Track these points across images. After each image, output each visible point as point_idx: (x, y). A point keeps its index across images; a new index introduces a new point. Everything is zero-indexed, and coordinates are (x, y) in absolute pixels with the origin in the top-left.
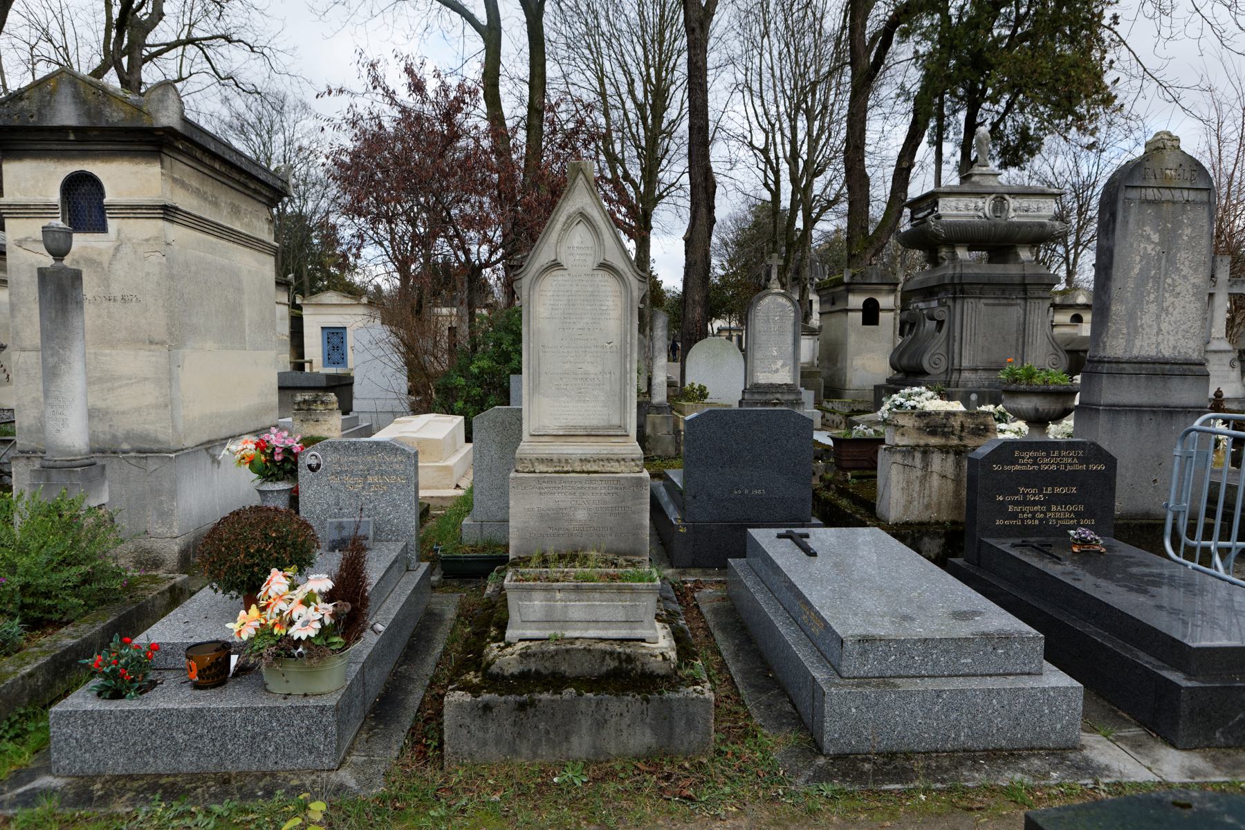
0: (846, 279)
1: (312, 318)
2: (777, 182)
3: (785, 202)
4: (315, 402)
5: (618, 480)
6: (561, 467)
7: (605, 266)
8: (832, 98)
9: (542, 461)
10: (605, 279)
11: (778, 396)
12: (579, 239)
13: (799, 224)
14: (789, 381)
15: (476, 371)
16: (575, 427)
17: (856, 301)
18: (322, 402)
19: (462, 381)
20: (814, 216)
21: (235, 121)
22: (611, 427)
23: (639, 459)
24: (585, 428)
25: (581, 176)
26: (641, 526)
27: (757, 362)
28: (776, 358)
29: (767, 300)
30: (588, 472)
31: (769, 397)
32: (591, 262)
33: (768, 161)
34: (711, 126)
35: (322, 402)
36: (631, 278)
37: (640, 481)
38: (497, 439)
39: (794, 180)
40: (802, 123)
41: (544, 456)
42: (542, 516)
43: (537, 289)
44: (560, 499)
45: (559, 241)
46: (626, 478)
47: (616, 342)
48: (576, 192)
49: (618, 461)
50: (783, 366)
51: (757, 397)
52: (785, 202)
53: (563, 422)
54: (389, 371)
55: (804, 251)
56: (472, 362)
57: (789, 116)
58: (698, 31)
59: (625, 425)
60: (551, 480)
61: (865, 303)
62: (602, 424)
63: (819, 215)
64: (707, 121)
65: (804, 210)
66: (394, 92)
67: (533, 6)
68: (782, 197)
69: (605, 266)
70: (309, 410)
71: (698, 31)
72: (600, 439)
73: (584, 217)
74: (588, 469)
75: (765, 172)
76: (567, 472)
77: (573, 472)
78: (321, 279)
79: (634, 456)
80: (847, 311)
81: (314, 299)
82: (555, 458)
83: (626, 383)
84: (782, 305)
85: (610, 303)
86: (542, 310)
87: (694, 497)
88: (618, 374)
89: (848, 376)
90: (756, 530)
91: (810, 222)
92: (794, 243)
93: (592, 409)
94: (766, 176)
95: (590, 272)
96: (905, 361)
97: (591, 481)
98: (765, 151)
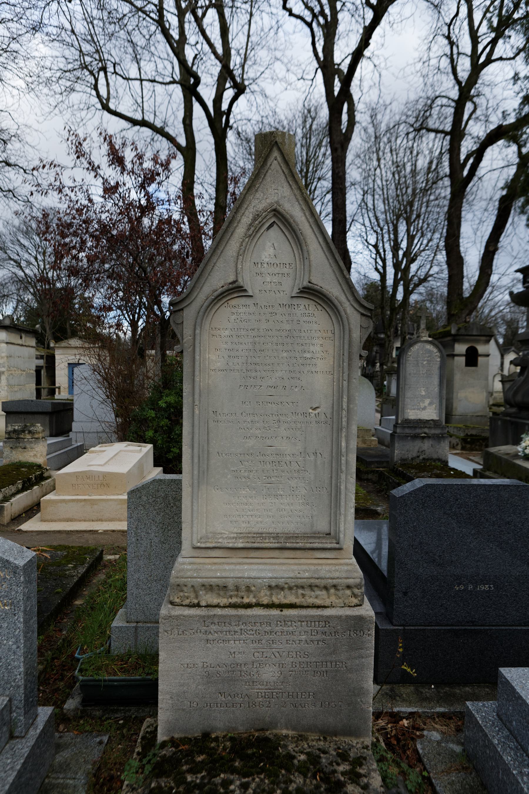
0: (453, 332)
1: (62, 356)
2: (384, 267)
3: (390, 281)
4: (23, 431)
5: (327, 620)
6: (239, 599)
7: (310, 292)
8: (423, 209)
9: (210, 588)
10: (307, 309)
11: (426, 430)
12: (271, 251)
13: (400, 296)
14: (435, 417)
15: (164, 405)
16: (260, 534)
17: (461, 348)
18: (30, 432)
19: (152, 414)
20: (410, 289)
21: (22, 226)
22: (315, 535)
23: (358, 586)
24: (276, 536)
25: (276, 154)
26: (360, 692)
27: (408, 401)
28: (424, 397)
29: (416, 347)
30: (281, 606)
31: (418, 431)
32: (289, 286)
33: (378, 252)
34: (349, 219)
35: (30, 432)
36: (350, 310)
37: (359, 622)
38: (158, 519)
39: (397, 266)
40: (402, 228)
41: (214, 581)
42: (209, 675)
43: (207, 326)
44: (234, 648)
45: (241, 253)
46: (339, 618)
47: (325, 407)
48: (268, 178)
49: (326, 588)
50: (430, 404)
51: (407, 431)
52: (390, 281)
53: (244, 528)
54: (95, 403)
55: (404, 313)
56: (161, 398)
57: (393, 223)
58: (339, 150)
59: (337, 532)
60: (224, 620)
61: (468, 350)
62: (302, 529)
63: (414, 289)
64: (345, 217)
65: (404, 285)
66: (99, 167)
67: (219, 132)
68: (388, 277)
69: (310, 292)
70: (18, 438)
71: (339, 150)
72: (298, 554)
73: (279, 217)
74: (280, 600)
75: (376, 259)
76: (249, 606)
77: (258, 605)
78: (81, 331)
79: (351, 581)
80: (453, 356)
81: (64, 344)
82: (230, 583)
83: (339, 471)
84: (430, 351)
85: (318, 348)
86: (213, 357)
87: (405, 594)
88: (327, 455)
89: (455, 405)
90: (507, 669)
91: (407, 293)
92: (396, 308)
93: (287, 510)
94: (376, 262)
95: (286, 300)
96: (519, 398)
97: (285, 621)
98: (376, 246)
